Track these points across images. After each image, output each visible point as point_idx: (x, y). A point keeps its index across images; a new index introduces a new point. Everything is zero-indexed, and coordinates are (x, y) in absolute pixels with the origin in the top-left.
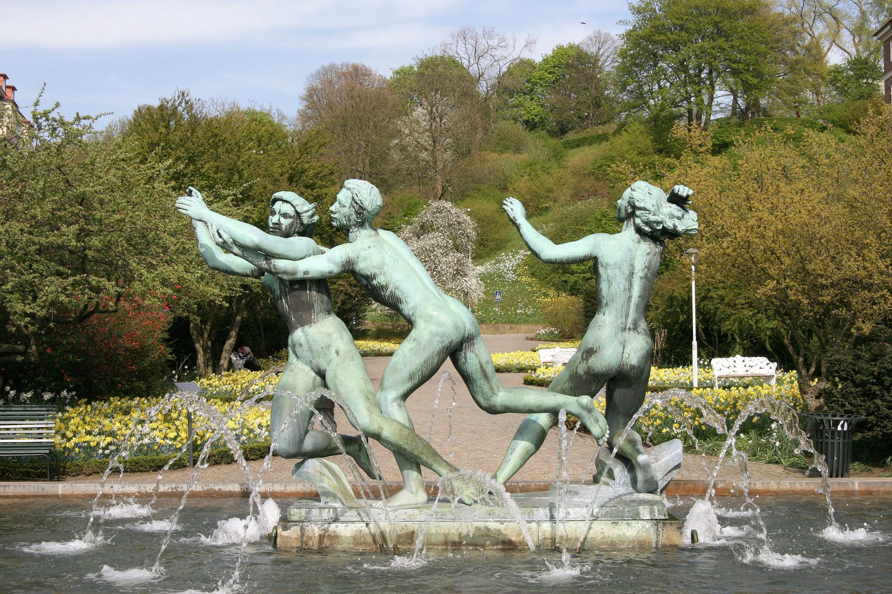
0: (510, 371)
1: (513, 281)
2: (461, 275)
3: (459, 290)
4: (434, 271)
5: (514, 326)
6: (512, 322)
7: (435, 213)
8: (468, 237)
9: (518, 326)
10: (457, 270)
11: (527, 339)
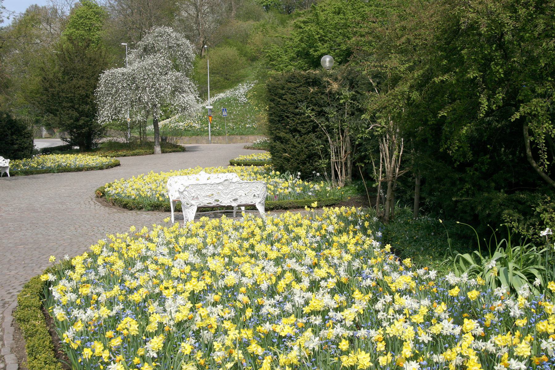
0: (141, 208)
1: (244, 103)
2: (179, 92)
3: (177, 105)
4: (152, 87)
5: (243, 137)
6: (242, 134)
7: (157, 36)
8: (187, 58)
9: (247, 137)
10: (175, 87)
11: (245, 148)
